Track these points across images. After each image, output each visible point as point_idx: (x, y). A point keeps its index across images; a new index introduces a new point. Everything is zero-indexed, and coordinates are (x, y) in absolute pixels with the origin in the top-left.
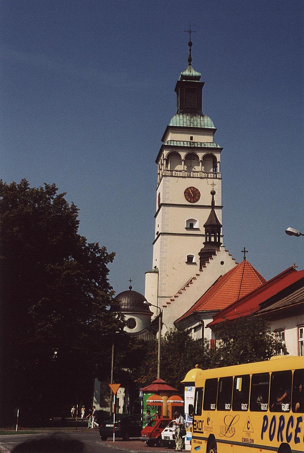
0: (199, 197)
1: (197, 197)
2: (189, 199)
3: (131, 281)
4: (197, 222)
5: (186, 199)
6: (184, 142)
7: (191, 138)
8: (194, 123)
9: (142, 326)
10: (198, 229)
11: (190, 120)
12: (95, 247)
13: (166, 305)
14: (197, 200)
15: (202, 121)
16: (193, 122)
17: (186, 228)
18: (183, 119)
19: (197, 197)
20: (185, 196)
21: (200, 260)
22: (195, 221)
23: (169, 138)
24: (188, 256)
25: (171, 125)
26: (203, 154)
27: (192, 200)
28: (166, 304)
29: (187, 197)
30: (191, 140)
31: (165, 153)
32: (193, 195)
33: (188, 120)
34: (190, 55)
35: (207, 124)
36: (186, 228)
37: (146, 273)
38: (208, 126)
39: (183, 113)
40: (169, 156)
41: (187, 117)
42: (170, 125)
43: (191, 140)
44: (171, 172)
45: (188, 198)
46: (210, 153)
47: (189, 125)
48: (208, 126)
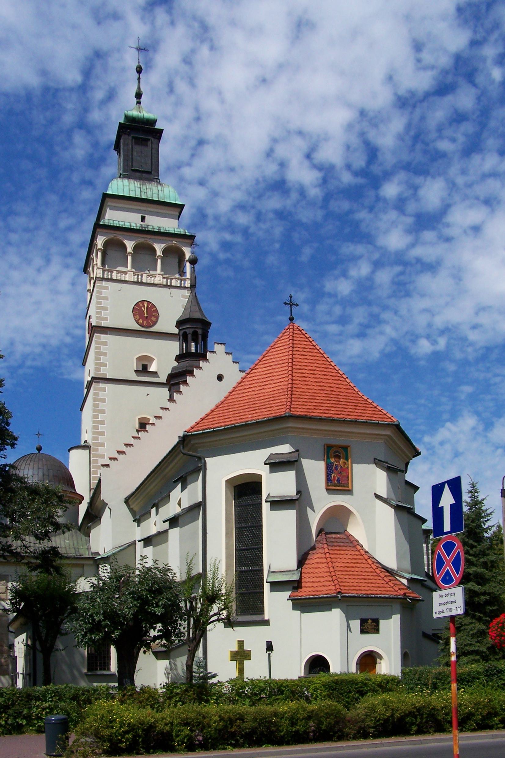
0: (157, 317)
1: (154, 319)
2: (141, 321)
3: (39, 434)
4: (155, 361)
5: (135, 320)
6: (92, 488)
7: (143, 219)
8: (147, 193)
9: (54, 342)
10: (155, 374)
11: (140, 188)
12: (111, 756)
13: (116, 455)
14: (154, 323)
15: (160, 192)
16: (145, 191)
17: (135, 371)
18: (129, 186)
19: (154, 319)
20: (134, 315)
21: (169, 392)
22: (151, 360)
23: (107, 216)
24: (139, 419)
25: (109, 192)
26: (163, 245)
27: (145, 323)
28: (117, 454)
29: (138, 317)
30: (142, 221)
31: (100, 241)
32: (147, 314)
33: (136, 188)
34: (139, 88)
35: (168, 197)
36: (135, 371)
37: (69, 450)
38: (170, 200)
39: (128, 177)
40: (106, 244)
41: (134, 183)
42: (108, 192)
43: (142, 221)
44: (109, 273)
45: (139, 319)
46: (174, 243)
47: (140, 195)
48: (170, 200)
